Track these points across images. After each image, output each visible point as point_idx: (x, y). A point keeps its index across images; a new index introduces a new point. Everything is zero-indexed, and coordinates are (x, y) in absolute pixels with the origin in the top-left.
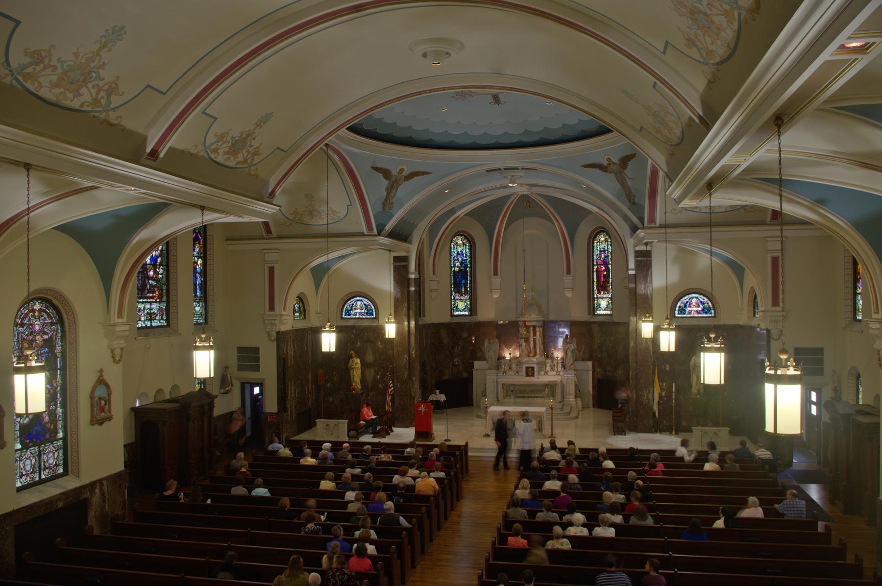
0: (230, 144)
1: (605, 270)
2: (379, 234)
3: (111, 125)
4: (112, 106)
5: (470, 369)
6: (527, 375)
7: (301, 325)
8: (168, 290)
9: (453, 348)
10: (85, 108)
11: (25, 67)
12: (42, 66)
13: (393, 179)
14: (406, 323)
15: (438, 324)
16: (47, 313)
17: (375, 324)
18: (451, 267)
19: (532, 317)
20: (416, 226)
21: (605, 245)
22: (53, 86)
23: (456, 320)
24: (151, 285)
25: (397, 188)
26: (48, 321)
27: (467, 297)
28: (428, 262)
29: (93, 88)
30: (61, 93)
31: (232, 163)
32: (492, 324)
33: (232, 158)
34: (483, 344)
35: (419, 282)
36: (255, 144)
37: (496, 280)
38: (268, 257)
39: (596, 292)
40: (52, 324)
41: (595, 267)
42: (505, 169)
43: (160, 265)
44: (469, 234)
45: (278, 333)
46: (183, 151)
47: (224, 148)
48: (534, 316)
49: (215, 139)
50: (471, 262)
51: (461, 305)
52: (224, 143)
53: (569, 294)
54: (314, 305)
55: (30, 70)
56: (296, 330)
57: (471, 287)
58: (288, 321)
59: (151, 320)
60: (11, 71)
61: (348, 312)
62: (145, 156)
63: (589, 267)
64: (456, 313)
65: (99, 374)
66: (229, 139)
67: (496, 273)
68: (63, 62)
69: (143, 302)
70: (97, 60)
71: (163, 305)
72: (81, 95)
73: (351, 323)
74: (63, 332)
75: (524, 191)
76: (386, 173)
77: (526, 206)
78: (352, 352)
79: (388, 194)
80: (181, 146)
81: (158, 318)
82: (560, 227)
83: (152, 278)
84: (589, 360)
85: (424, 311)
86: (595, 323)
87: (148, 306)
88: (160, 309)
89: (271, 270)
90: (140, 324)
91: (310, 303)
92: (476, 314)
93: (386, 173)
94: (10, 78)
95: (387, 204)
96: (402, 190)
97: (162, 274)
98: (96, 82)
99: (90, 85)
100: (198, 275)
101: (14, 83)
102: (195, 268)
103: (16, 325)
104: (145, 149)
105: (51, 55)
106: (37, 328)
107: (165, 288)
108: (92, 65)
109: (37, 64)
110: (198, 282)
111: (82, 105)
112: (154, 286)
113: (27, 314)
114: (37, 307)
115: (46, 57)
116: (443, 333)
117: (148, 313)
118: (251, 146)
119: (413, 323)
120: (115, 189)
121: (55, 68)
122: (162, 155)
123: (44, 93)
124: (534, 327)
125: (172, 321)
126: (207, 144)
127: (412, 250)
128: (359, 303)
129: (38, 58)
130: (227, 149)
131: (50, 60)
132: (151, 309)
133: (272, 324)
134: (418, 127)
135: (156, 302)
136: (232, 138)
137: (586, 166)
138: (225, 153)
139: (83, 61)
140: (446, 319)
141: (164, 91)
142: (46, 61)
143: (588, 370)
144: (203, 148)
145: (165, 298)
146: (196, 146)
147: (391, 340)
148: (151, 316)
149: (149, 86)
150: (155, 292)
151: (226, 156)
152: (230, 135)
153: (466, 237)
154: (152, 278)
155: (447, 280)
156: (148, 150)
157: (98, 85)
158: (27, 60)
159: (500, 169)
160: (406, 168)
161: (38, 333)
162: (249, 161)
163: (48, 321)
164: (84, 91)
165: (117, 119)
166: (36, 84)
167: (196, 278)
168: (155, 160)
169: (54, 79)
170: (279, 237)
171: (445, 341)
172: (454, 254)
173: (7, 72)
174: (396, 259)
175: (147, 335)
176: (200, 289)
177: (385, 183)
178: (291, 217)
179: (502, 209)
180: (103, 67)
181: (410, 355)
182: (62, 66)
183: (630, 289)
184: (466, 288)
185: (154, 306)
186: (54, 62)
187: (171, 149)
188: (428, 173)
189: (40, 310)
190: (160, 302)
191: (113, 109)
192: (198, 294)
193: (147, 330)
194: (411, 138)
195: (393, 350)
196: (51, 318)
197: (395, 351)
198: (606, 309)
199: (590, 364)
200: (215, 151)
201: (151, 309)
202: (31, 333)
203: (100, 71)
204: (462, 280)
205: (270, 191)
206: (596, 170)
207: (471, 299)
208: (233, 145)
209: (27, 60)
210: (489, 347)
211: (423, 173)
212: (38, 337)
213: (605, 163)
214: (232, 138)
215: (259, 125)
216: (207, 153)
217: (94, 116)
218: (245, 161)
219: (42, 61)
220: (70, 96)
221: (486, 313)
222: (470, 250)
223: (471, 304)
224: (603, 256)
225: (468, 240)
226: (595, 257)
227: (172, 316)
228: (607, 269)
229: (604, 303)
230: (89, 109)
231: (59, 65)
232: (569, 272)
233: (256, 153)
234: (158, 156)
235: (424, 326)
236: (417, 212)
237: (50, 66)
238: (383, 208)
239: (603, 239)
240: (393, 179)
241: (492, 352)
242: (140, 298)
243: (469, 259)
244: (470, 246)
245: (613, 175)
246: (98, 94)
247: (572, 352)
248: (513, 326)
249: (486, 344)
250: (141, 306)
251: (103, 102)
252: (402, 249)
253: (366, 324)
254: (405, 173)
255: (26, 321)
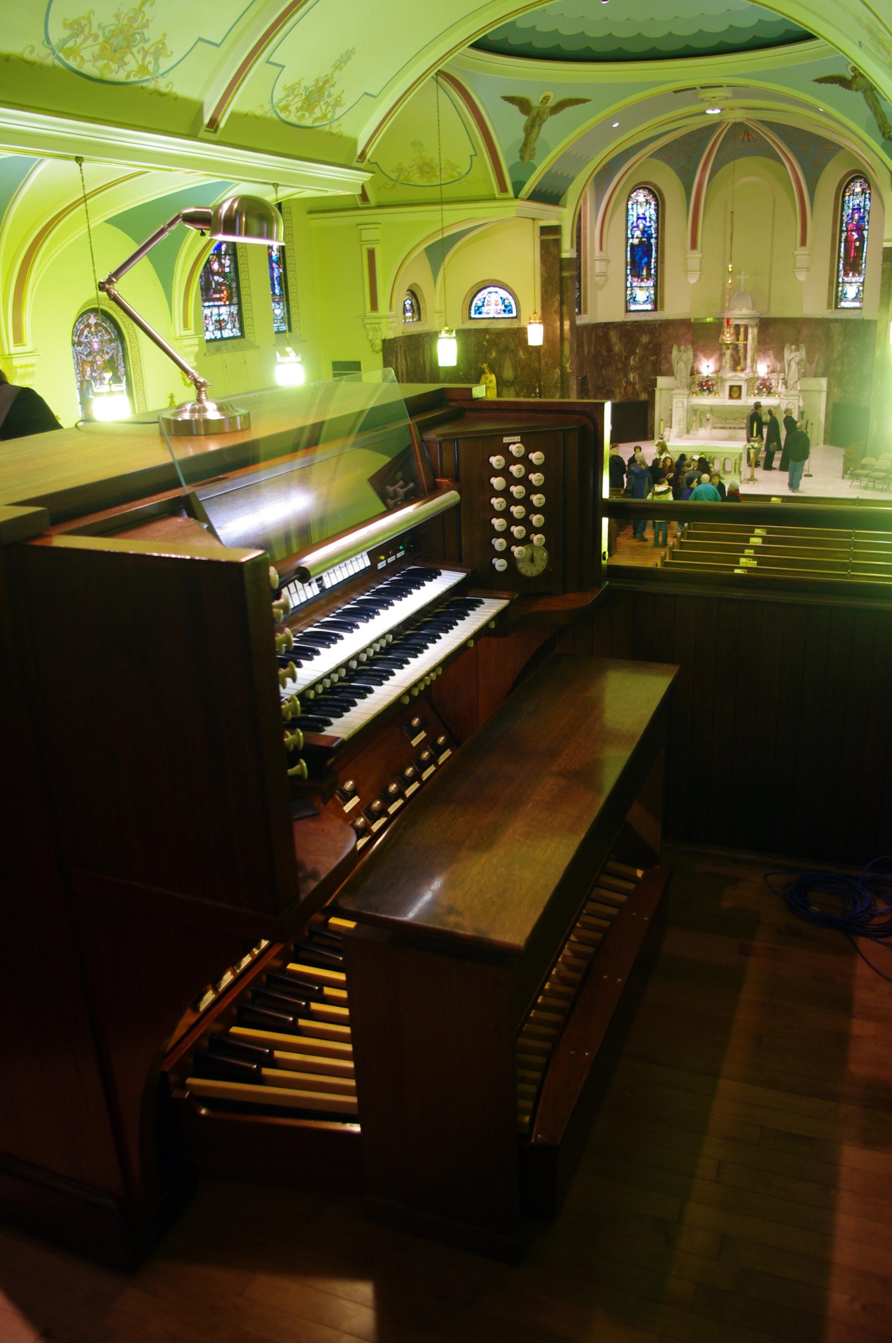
0: (303, 97)
1: (857, 240)
2: (516, 197)
3: (162, 95)
4: (161, 72)
5: (651, 388)
6: (731, 397)
7: (415, 329)
8: (238, 288)
9: (627, 358)
10: (132, 79)
11: (65, 41)
12: (82, 37)
13: (534, 113)
14: (558, 324)
15: (607, 325)
16: (104, 327)
17: (515, 325)
18: (627, 239)
19: (741, 312)
20: (572, 179)
21: (862, 199)
22: (97, 58)
23: (632, 317)
24: (217, 283)
25: (540, 125)
26: (107, 337)
27: (651, 283)
28: (592, 233)
29: (139, 52)
30: (105, 66)
31: (308, 122)
32: (685, 323)
33: (307, 115)
34: (671, 352)
35: (576, 264)
36: (335, 92)
37: (697, 254)
38: (366, 235)
39: (842, 273)
40: (111, 341)
41: (844, 235)
42: (702, 88)
43: (225, 255)
44: (655, 186)
45: (384, 341)
46: (246, 115)
47: (297, 103)
48: (745, 312)
49: (285, 93)
50: (657, 229)
51: (641, 295)
52: (296, 96)
53: (801, 277)
54: (432, 301)
55: (71, 44)
56: (408, 336)
57: (656, 267)
58: (394, 324)
59: (220, 329)
60: (52, 49)
61: (478, 310)
62: (204, 128)
63: (834, 235)
64: (633, 307)
65: (169, 400)
66: (302, 91)
67: (694, 246)
68: (104, 28)
69: (209, 307)
70: (140, 19)
71: (234, 309)
72: (126, 64)
73: (482, 325)
74: (124, 350)
75: (738, 116)
76: (523, 105)
77: (742, 140)
78: (485, 366)
79: (528, 135)
80: (244, 109)
81: (229, 326)
82: (792, 166)
83: (218, 274)
84: (823, 376)
85: (586, 307)
86: (836, 320)
87: (215, 311)
88: (231, 315)
89: (371, 254)
90: (209, 335)
91: (426, 297)
92: (662, 308)
93: (523, 105)
94: (52, 57)
95: (526, 149)
96: (550, 126)
97: (229, 267)
98: (141, 45)
99: (135, 50)
100: (274, 265)
101: (57, 63)
102: (270, 256)
103: (74, 344)
104: (202, 121)
105: (90, 22)
106: (96, 346)
107: (234, 285)
108: (135, 25)
109: (77, 35)
110: (276, 275)
111: (128, 76)
112: (221, 284)
113: (83, 331)
114: (93, 320)
115: (86, 25)
116: (614, 336)
117: (216, 321)
118: (330, 96)
119: (567, 325)
120: (172, 170)
121: (96, 37)
122: (222, 125)
123: (88, 69)
124: (746, 328)
125: (247, 330)
126: (275, 101)
127: (562, 216)
128: (493, 295)
129: (77, 28)
130: (299, 104)
131: (90, 29)
132: (219, 315)
133: (375, 330)
134: (655, 33)
135: (225, 305)
136: (306, 88)
137: (820, 81)
138: (298, 110)
139: (125, 22)
140: (617, 315)
141: (218, 42)
142: (86, 30)
143: (820, 391)
144: (270, 107)
145: (235, 300)
146: (262, 106)
147: (537, 349)
148: (220, 325)
149: (200, 39)
150: (222, 292)
151: (300, 113)
152: (302, 86)
153: (650, 192)
154: (218, 274)
155: (619, 257)
156: (206, 120)
157: (143, 48)
158: (66, 33)
159: (694, 89)
160: (551, 94)
161: (98, 353)
162: (329, 116)
163: (107, 337)
164: (128, 58)
165: (167, 86)
166: (78, 59)
167: (272, 269)
168: (215, 131)
169: (96, 49)
170: (379, 206)
171: (617, 348)
172: (632, 219)
173: (49, 51)
174: (545, 230)
175: (218, 350)
176: (280, 284)
177: (523, 119)
178: (394, 176)
179: (706, 145)
180: (146, 25)
181: (563, 369)
182: (104, 33)
183: (718, 327)
184: (649, 269)
185: (223, 310)
186: (95, 30)
187: (232, 114)
188: (584, 101)
189: (96, 324)
190: (230, 305)
191: (162, 75)
192: (277, 291)
193: (218, 343)
194: (588, 49)
195: (540, 362)
196: (110, 334)
197: (543, 363)
198: (854, 300)
199: (824, 381)
200: (286, 108)
201: (219, 315)
202: (89, 354)
203: (145, 30)
204: (643, 258)
205: (359, 152)
206: (836, 87)
207: (655, 286)
208: (307, 97)
209: (66, 33)
210: (680, 356)
211: (578, 101)
212: (98, 358)
213: (849, 75)
214: (306, 88)
215: (338, 66)
216: (275, 112)
217: (143, 88)
218: (324, 116)
219: (82, 31)
220: (114, 66)
221: (676, 308)
222: (657, 211)
223: (656, 294)
224: (856, 216)
225: (654, 196)
226: (845, 219)
227: (246, 323)
228: (861, 238)
229: (851, 291)
230: (136, 79)
231: (100, 33)
232: (803, 243)
233: (337, 103)
234: (218, 127)
235: (585, 327)
236: (573, 159)
237: (91, 35)
238: (522, 158)
239: (858, 189)
240: (534, 113)
241: (681, 364)
242: (205, 301)
243: (654, 225)
244: (657, 205)
245: (859, 95)
246: (144, 59)
247: (798, 364)
248: (718, 327)
249: (675, 352)
250: (207, 312)
251: (151, 68)
252: (550, 215)
253: (502, 325)
254: (551, 103)
255: (83, 339)
